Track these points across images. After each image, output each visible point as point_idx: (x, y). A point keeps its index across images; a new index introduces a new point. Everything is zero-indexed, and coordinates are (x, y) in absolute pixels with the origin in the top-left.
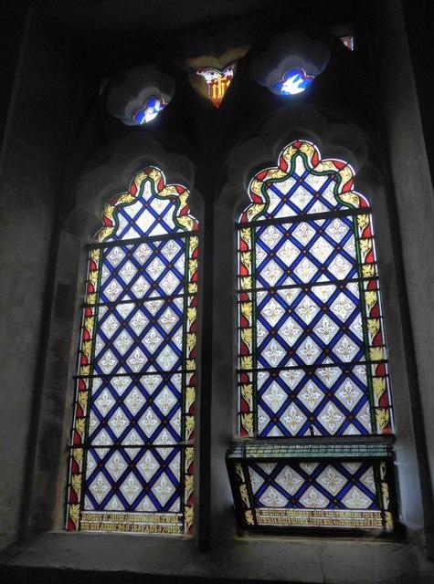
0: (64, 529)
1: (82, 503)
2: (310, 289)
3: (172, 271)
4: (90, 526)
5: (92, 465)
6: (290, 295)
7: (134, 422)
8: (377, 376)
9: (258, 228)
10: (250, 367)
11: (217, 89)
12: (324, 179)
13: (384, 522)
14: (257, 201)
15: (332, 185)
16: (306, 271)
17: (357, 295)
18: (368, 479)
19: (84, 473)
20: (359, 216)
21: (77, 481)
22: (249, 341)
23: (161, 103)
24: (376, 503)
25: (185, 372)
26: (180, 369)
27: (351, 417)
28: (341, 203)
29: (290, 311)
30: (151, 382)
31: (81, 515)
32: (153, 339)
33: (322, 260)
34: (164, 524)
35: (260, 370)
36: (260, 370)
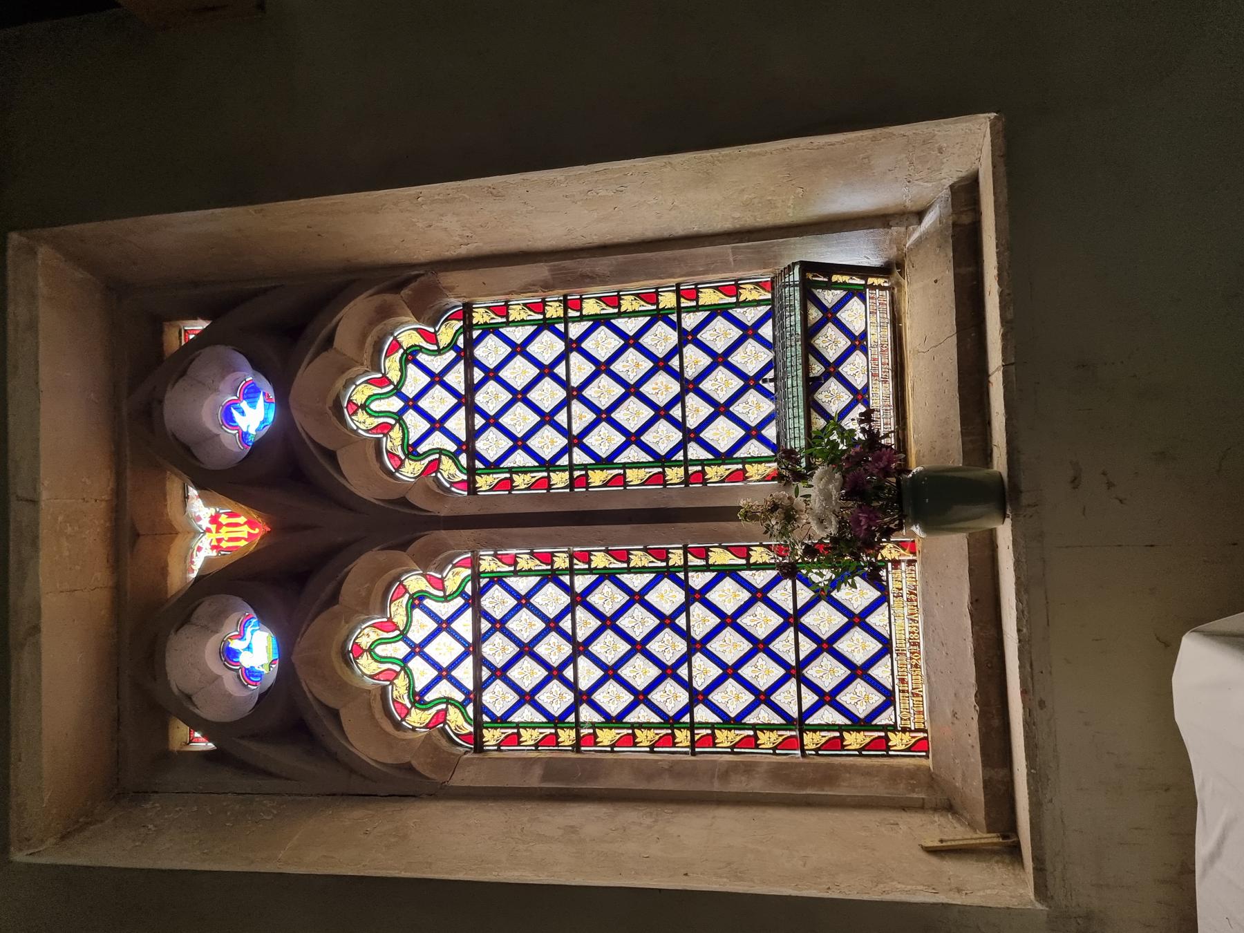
0: (927, 757)
1: (884, 728)
2: (578, 595)
3: (527, 592)
4: (919, 712)
5: (828, 715)
6: (581, 416)
7: (760, 646)
8: (697, 299)
9: (486, 718)
10: (681, 471)
11: (231, 540)
12: (412, 369)
13: (881, 288)
14: (442, 716)
15: (421, 357)
16: (548, 394)
17: (586, 325)
18: (830, 297)
19: (840, 728)
20: (475, 322)
21: (854, 740)
22: (643, 474)
23: (235, 637)
24: (854, 292)
25: (686, 568)
26: (681, 575)
27: (749, 332)
28: (453, 346)
29: (604, 416)
30: (701, 621)
31: (904, 730)
32: (638, 622)
33: (534, 372)
34: (905, 592)
35: (685, 455)
36: (685, 455)
